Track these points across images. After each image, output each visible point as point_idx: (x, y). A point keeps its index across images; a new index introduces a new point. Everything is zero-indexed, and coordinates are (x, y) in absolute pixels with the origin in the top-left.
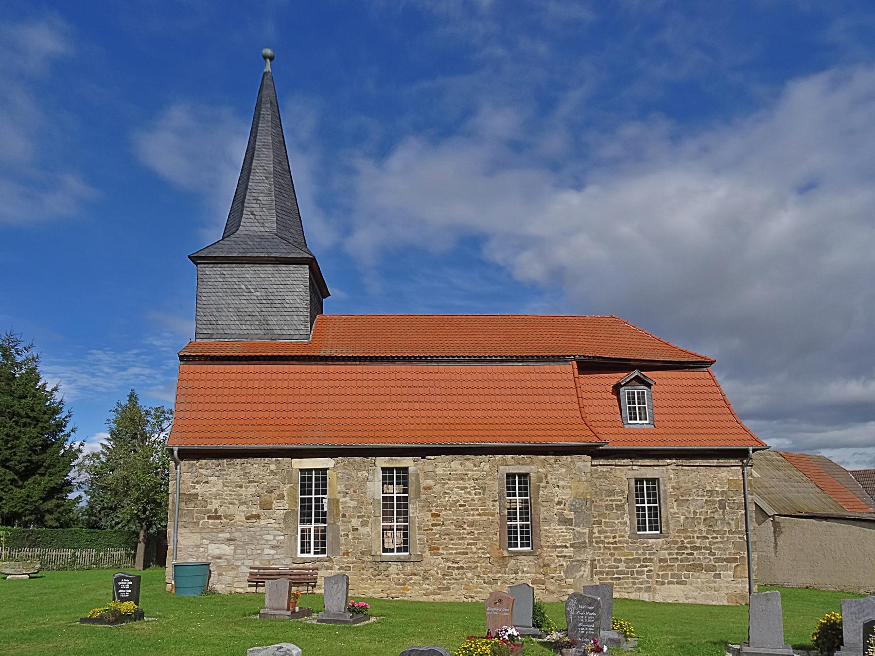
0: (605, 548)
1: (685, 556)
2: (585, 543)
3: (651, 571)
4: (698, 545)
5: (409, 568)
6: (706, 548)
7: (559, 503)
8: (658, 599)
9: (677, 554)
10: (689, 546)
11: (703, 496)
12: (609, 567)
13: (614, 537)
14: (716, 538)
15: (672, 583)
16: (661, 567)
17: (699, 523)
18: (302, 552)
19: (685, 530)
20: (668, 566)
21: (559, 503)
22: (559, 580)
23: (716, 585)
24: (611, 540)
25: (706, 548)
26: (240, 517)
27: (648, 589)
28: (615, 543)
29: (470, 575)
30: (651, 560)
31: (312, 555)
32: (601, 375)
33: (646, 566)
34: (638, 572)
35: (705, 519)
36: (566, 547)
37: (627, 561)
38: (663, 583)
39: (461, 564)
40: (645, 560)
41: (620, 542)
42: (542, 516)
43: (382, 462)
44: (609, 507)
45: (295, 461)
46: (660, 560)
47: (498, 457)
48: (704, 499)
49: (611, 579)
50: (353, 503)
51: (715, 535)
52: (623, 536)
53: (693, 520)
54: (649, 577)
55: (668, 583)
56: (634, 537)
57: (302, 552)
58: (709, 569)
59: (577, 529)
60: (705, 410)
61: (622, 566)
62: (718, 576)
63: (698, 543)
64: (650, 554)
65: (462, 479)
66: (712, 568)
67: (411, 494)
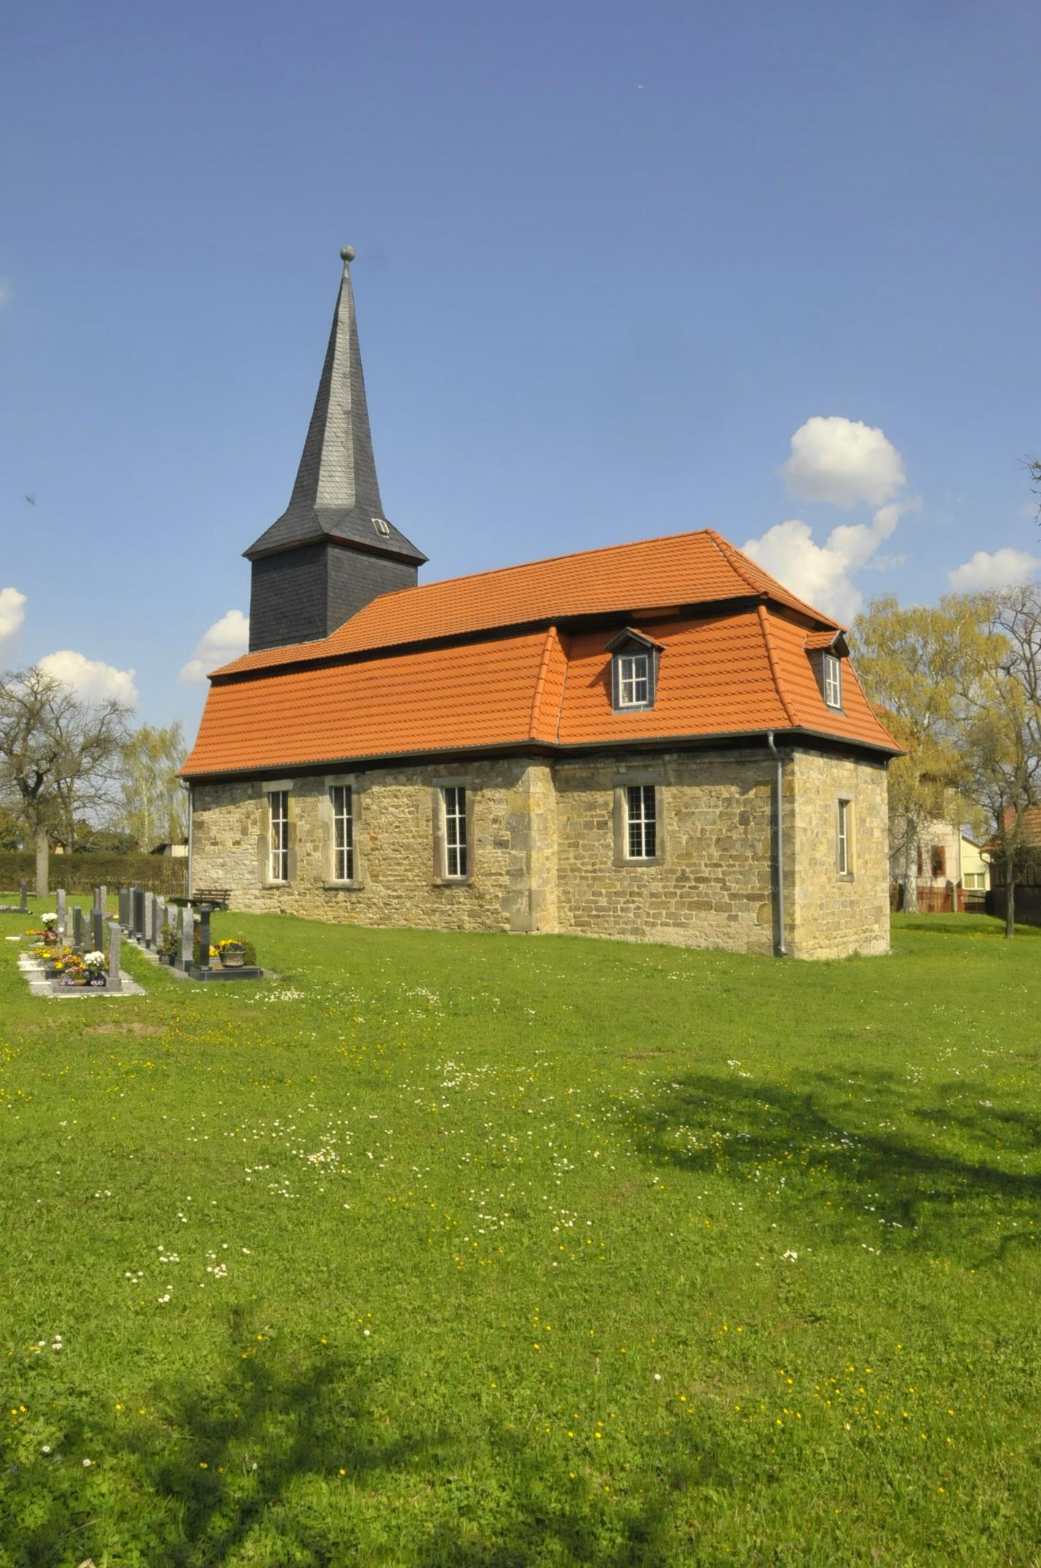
0: (582, 878)
1: (686, 889)
2: (521, 870)
3: (638, 908)
4: (706, 875)
5: (354, 897)
6: (717, 880)
7: (495, 821)
8: (648, 940)
9: (675, 887)
10: (692, 876)
11: (716, 806)
12: (587, 902)
13: (593, 864)
14: (733, 866)
15: (667, 925)
16: (652, 904)
17: (709, 846)
18: (632, 854)
19: (689, 855)
20: (663, 902)
21: (495, 821)
22: (495, 912)
23: (731, 931)
24: (589, 868)
25: (717, 880)
26: (229, 843)
27: (635, 931)
28: (594, 871)
29: (408, 904)
30: (639, 894)
31: (644, 857)
32: (711, 626)
33: (634, 902)
34: (622, 909)
35: (718, 840)
36: (501, 874)
37: (609, 895)
38: (654, 925)
39: (400, 892)
40: (631, 894)
41: (601, 871)
42: (476, 837)
43: (330, 781)
44: (588, 826)
45: (265, 784)
46: (652, 895)
47: (430, 768)
48: (718, 811)
49: (589, 916)
50: (308, 827)
51: (731, 862)
52: (605, 863)
53: (698, 842)
54: (637, 915)
55: (662, 925)
56: (619, 863)
57: (632, 854)
58: (720, 908)
59: (513, 852)
60: (728, 678)
61: (603, 902)
62: (735, 918)
63: (706, 872)
64: (638, 887)
65: (396, 796)
66: (726, 908)
67: (354, 816)
